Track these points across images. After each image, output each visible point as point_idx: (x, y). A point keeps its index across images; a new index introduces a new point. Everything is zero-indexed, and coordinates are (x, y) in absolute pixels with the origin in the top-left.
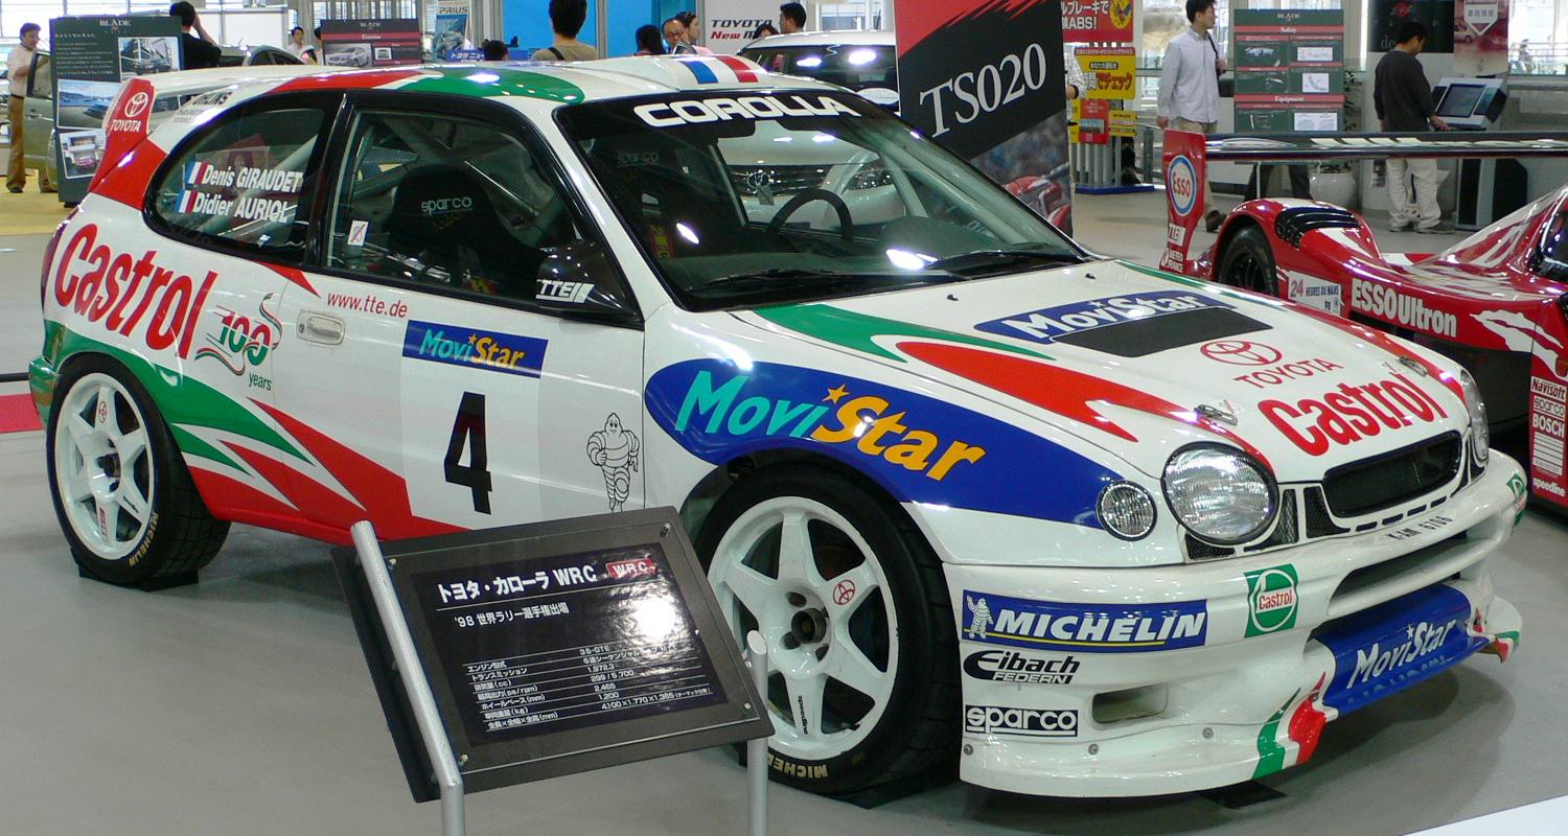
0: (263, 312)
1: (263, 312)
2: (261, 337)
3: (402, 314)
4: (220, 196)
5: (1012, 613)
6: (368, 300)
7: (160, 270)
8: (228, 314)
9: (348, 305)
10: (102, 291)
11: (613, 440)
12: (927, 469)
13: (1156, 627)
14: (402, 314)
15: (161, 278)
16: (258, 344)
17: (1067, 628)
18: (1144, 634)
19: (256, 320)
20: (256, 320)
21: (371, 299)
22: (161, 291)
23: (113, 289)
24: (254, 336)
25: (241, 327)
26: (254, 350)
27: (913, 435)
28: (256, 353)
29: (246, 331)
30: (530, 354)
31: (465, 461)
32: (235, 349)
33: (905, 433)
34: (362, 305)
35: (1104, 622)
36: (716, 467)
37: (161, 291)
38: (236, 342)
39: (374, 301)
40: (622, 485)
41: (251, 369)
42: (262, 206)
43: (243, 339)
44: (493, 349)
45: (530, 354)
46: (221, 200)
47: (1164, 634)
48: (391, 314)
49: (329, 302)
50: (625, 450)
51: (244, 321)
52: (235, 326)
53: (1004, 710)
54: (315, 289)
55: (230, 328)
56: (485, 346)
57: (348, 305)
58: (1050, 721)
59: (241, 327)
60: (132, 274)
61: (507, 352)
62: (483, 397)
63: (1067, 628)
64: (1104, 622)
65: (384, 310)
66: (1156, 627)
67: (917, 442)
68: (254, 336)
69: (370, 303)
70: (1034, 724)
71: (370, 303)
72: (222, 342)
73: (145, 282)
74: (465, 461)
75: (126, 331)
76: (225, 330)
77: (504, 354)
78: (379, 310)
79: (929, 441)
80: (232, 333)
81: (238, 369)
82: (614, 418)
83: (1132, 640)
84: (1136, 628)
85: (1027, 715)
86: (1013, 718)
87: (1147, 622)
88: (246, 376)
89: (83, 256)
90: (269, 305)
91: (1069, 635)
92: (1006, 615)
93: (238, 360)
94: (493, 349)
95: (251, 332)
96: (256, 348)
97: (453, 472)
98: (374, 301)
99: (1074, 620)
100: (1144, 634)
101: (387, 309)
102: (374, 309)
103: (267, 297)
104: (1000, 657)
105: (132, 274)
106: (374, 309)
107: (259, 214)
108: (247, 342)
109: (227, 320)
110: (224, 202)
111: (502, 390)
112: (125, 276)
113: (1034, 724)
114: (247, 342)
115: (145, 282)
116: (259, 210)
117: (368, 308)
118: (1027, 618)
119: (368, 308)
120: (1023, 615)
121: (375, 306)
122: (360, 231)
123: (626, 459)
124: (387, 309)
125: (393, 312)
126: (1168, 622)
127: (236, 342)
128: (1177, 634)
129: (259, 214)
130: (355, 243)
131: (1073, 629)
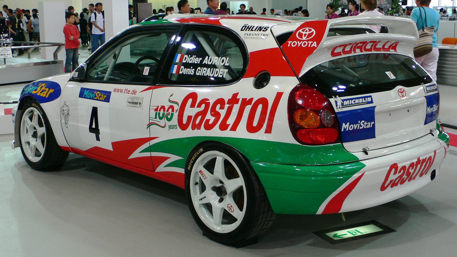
0: (170, 101)
1: (170, 101)
3: (135, 93)
4: (195, 56)
5: (346, 101)
6: (125, 90)
7: (244, 100)
8: (156, 107)
9: (120, 91)
11: (65, 108)
14: (129, 93)
15: (245, 102)
16: (170, 113)
17: (354, 102)
18: (364, 101)
19: (167, 105)
20: (167, 105)
21: (126, 89)
23: (217, 115)
24: (168, 111)
25: (162, 110)
26: (168, 116)
28: (169, 117)
29: (164, 111)
30: (106, 97)
31: (94, 126)
32: (161, 118)
34: (124, 91)
38: (161, 116)
39: (127, 90)
41: (169, 123)
42: (205, 70)
43: (163, 114)
45: (106, 97)
46: (196, 58)
48: (132, 94)
49: (114, 91)
51: (163, 107)
52: (160, 111)
54: (33, 80)
55: (158, 112)
57: (120, 91)
59: (162, 110)
62: (97, 108)
63: (354, 102)
65: (130, 93)
68: (168, 111)
69: (126, 91)
71: (126, 91)
72: (156, 118)
73: (236, 108)
74: (94, 126)
76: (156, 114)
77: (102, 96)
78: (129, 93)
80: (159, 114)
81: (163, 125)
88: (167, 127)
89: (193, 106)
92: (345, 102)
93: (162, 122)
95: (166, 111)
96: (169, 115)
97: (91, 130)
98: (127, 90)
101: (131, 92)
102: (127, 92)
103: (172, 95)
105: (227, 106)
106: (127, 92)
107: (204, 73)
108: (165, 114)
109: (156, 110)
110: (197, 58)
111: (100, 105)
114: (165, 114)
115: (236, 108)
116: (204, 72)
117: (125, 92)
118: (348, 101)
119: (125, 92)
120: (347, 101)
121: (127, 91)
122: (147, 70)
123: (67, 113)
124: (131, 92)
125: (133, 93)
127: (161, 116)
129: (204, 73)
130: (146, 74)
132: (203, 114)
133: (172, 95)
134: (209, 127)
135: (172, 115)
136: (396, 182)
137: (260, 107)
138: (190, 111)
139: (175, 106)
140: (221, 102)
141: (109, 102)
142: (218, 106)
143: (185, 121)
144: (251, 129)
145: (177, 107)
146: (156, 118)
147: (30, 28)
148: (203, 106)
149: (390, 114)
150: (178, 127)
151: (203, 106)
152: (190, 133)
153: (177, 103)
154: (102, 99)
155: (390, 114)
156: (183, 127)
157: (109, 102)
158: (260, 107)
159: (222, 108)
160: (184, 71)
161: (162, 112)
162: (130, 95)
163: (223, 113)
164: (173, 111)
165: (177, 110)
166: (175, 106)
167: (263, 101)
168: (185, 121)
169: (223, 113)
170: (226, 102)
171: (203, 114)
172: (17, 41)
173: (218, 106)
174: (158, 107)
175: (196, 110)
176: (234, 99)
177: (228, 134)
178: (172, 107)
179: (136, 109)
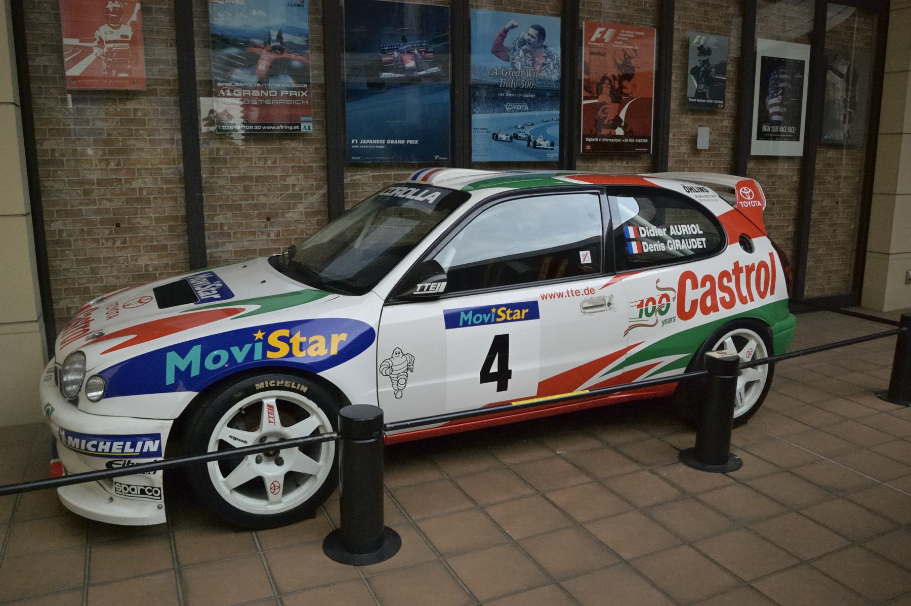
2: (664, 301)
7: (747, 267)
8: (639, 303)
10: (719, 294)
12: (329, 350)
13: (133, 446)
15: (750, 269)
17: (93, 446)
19: (657, 295)
20: (657, 295)
22: (753, 275)
25: (651, 303)
27: (312, 339)
28: (663, 309)
31: (494, 369)
33: (308, 339)
35: (108, 444)
36: (196, 394)
37: (753, 275)
38: (650, 311)
40: (402, 381)
43: (654, 308)
44: (509, 312)
47: (138, 449)
50: (406, 363)
51: (652, 300)
52: (647, 305)
53: (129, 486)
56: (504, 312)
58: (149, 491)
59: (651, 303)
60: (733, 277)
61: (518, 311)
63: (93, 446)
64: (108, 444)
66: (133, 446)
67: (316, 342)
68: (660, 301)
70: (143, 492)
73: (743, 276)
74: (494, 369)
75: (752, 300)
79: (321, 339)
80: (646, 309)
82: (398, 350)
83: (123, 452)
84: (124, 446)
85: (139, 488)
86: (133, 490)
87: (128, 444)
89: (695, 286)
90: (660, 285)
91: (94, 450)
93: (651, 320)
94: (509, 312)
99: (95, 442)
100: (128, 449)
104: (122, 463)
105: (733, 277)
109: (640, 306)
112: (729, 281)
113: (143, 492)
115: (743, 276)
126: (140, 444)
128: (145, 450)
131: (96, 446)
132: (712, 292)
133: (658, 281)
134: (729, 305)
135: (668, 305)
136: (259, 307)
137: (763, 270)
138: (692, 295)
139: (669, 293)
140: (724, 274)
141: (538, 317)
142: (725, 280)
143: (687, 308)
144: (762, 295)
145: (672, 295)
146: (641, 316)
147: (513, 92)
148: (708, 284)
149: (264, 282)
150: (677, 318)
151: (708, 284)
152: (700, 319)
153: (672, 289)
154: (518, 317)
155: (264, 282)
156: (683, 315)
157: (538, 317)
158: (763, 270)
159: (729, 281)
160: (649, 248)
161: (648, 308)
162: (582, 298)
163: (732, 285)
164: (668, 299)
165: (674, 299)
166: (669, 293)
167: (762, 264)
168: (687, 308)
169: (732, 285)
170: (731, 273)
171: (712, 292)
172: (802, 80)
173: (725, 280)
174: (642, 301)
175: (701, 291)
176: (737, 269)
177: (750, 306)
178: (666, 296)
179: (599, 316)
